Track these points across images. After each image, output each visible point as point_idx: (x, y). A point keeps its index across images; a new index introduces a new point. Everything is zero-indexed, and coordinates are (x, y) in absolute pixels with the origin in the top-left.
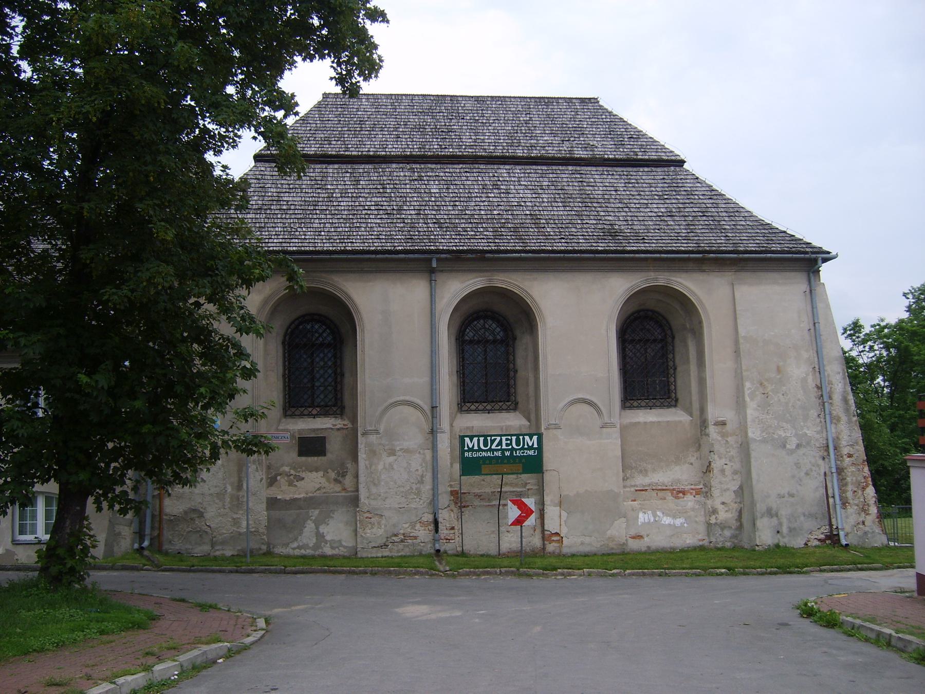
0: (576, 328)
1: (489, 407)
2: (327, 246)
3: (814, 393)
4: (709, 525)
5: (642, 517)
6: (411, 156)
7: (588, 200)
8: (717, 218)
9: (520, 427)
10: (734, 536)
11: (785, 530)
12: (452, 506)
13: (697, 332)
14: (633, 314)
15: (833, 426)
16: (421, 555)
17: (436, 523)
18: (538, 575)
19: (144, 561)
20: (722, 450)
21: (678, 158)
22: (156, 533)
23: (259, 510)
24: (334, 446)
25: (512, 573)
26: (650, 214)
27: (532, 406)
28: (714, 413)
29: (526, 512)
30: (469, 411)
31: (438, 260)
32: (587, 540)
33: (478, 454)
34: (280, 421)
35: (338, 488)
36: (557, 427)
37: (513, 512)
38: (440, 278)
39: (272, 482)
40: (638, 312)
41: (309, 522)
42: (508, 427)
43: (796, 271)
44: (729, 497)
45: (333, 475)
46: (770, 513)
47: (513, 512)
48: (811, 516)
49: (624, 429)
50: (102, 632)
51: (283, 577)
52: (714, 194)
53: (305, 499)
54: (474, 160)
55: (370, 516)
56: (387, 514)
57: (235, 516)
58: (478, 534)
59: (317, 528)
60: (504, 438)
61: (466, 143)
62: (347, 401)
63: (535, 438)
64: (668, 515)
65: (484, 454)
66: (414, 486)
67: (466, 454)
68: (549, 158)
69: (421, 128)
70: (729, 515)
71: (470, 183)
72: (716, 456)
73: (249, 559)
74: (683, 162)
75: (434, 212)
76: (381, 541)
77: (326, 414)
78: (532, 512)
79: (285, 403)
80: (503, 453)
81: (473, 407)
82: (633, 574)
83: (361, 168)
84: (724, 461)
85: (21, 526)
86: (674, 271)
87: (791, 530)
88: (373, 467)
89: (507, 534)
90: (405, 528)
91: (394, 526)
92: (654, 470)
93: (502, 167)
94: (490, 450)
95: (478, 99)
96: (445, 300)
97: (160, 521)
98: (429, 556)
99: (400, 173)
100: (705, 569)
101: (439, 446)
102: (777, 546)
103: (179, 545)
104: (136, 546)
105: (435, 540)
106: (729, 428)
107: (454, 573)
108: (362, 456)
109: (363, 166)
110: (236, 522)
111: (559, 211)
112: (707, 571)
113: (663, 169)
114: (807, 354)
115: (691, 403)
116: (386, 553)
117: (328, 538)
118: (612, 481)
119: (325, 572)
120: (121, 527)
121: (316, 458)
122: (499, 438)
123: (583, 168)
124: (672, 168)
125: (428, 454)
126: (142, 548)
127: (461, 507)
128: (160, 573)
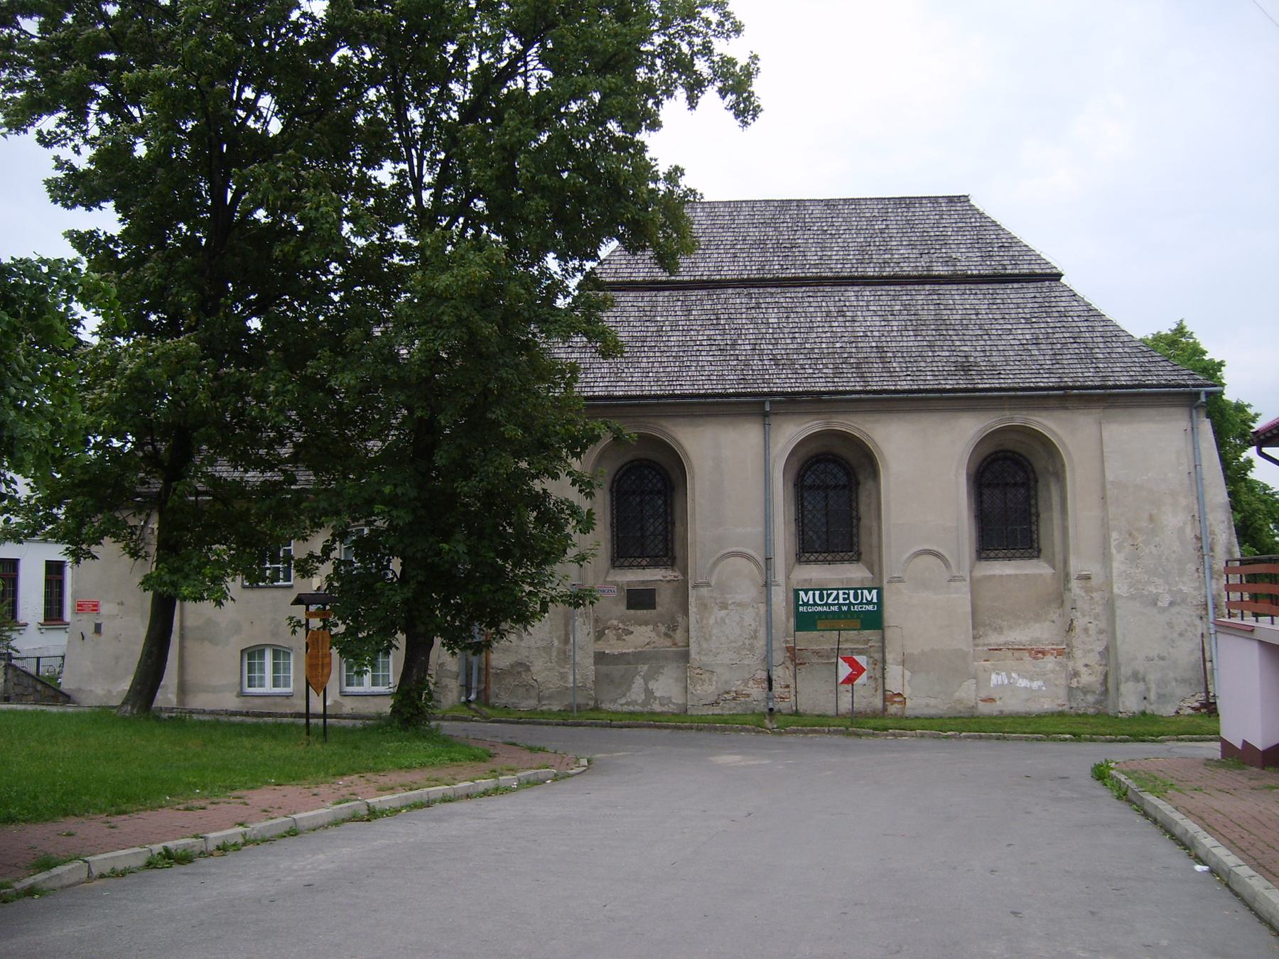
0: (923, 474)
1: (829, 558)
2: (656, 390)
3: (1192, 545)
4: (1070, 689)
5: (995, 679)
6: (749, 280)
7: (943, 327)
8: (1090, 345)
9: (862, 580)
10: (1098, 702)
11: (1153, 696)
12: (788, 663)
13: (1059, 476)
14: (989, 456)
15: (1214, 581)
16: (753, 713)
17: (770, 680)
18: (867, 735)
19: (472, 713)
21: (1055, 271)
22: (483, 686)
23: (588, 667)
24: (665, 599)
25: (841, 732)
27: (875, 557)
28: (1075, 566)
29: (858, 670)
30: (808, 562)
31: (771, 402)
32: (932, 702)
35: (668, 642)
36: (900, 580)
37: (845, 670)
38: (774, 421)
39: (600, 635)
40: (996, 453)
42: (849, 580)
43: (1176, 406)
44: (1093, 659)
45: (663, 629)
46: (1136, 677)
47: (845, 670)
48: (1184, 681)
49: (975, 585)
50: (452, 760)
51: (608, 730)
52: (1092, 314)
53: (634, 654)
54: (819, 281)
56: (718, 670)
58: (814, 693)
59: (646, 684)
61: (810, 261)
62: (678, 553)
63: (874, 592)
64: (1024, 677)
65: (820, 609)
66: (747, 642)
67: (801, 609)
68: (903, 277)
69: (761, 244)
70: (1093, 679)
71: (812, 309)
72: (1078, 614)
73: (576, 714)
74: (1060, 275)
76: (712, 699)
77: (656, 566)
78: (864, 670)
79: (613, 553)
81: (812, 558)
82: (969, 737)
83: (694, 295)
85: (250, 679)
86: (1033, 409)
87: (1160, 696)
90: (737, 685)
91: (726, 682)
92: (1010, 628)
93: (849, 288)
95: (829, 204)
96: (780, 446)
97: (487, 675)
98: (762, 714)
99: (736, 299)
100: (1047, 734)
101: (774, 599)
102: (1144, 713)
103: (504, 699)
104: (463, 699)
105: (769, 699)
106: (1093, 582)
107: (781, 731)
108: (692, 609)
109: (696, 292)
110: (563, 677)
111: (909, 342)
112: (1049, 736)
113: (1035, 285)
115: (1053, 554)
116: (717, 710)
117: (657, 694)
118: (961, 640)
119: (650, 726)
124: (1047, 283)
125: (762, 608)
127: (796, 665)
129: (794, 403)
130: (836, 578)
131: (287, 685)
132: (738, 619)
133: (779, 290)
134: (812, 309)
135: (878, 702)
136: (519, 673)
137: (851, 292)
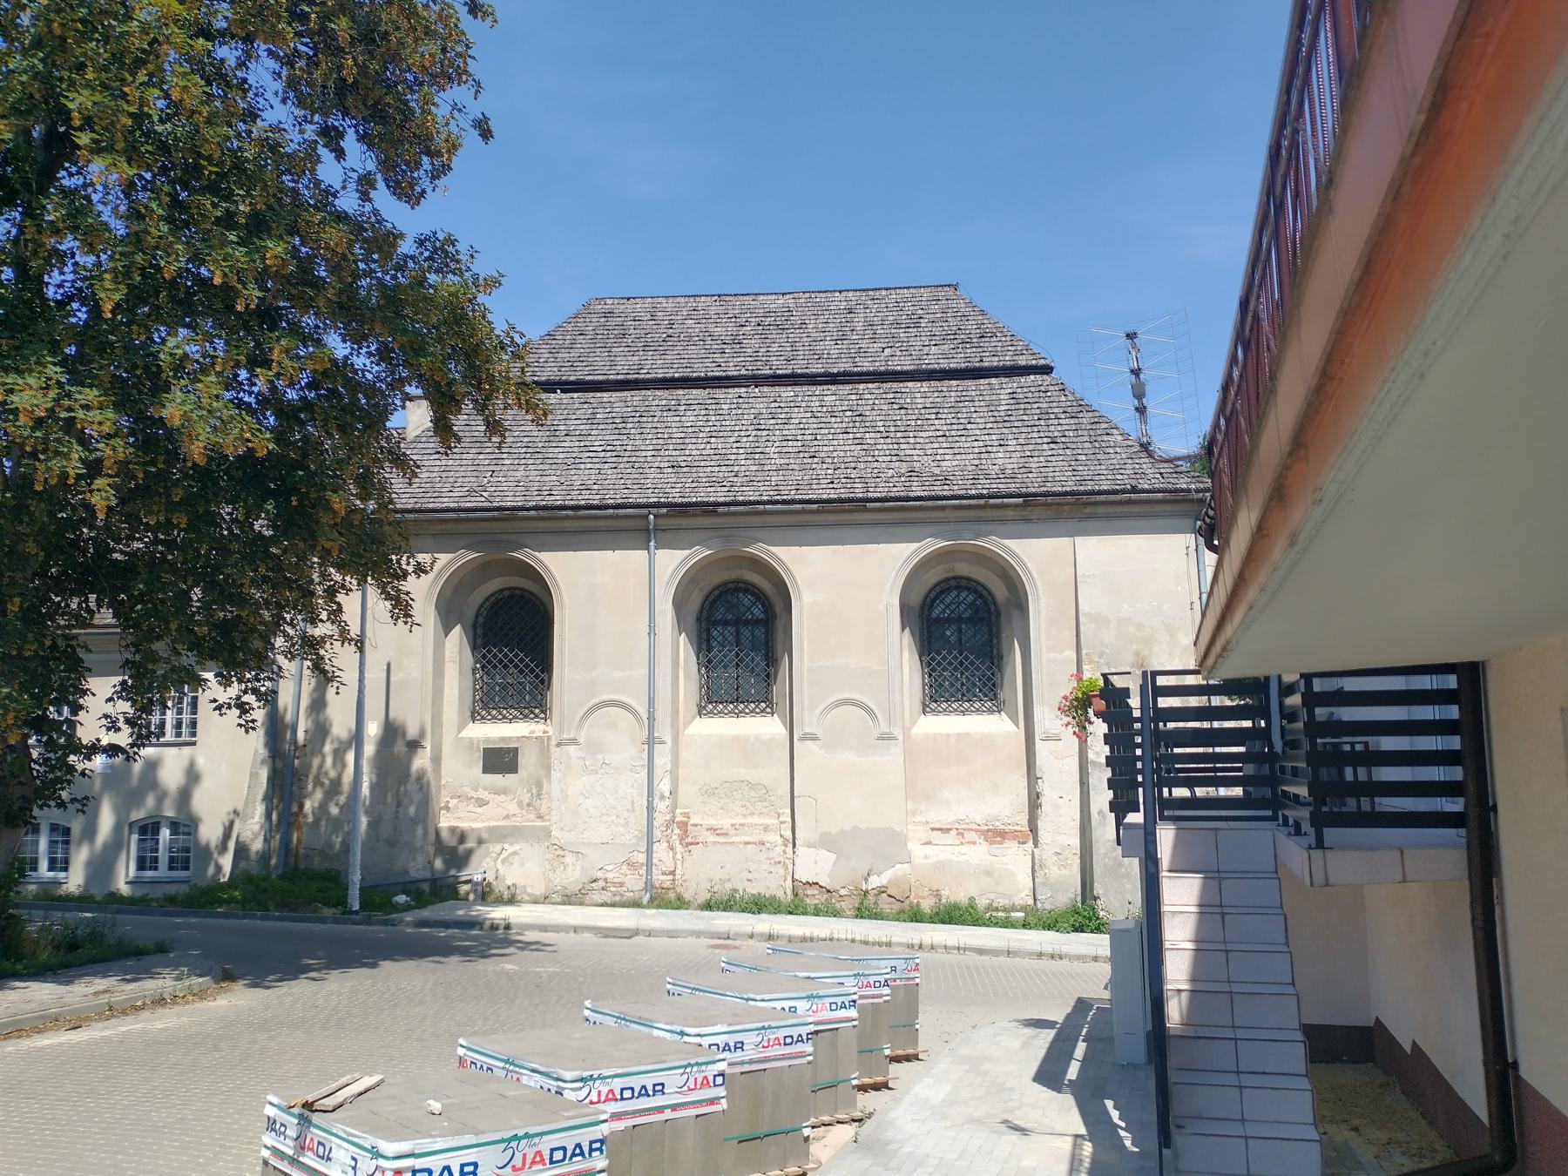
0: (847, 598)
24: (527, 760)
34: (461, 728)
101: (657, 761)
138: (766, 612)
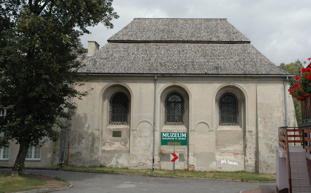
0: (203, 98)
6: (157, 41)
13: (244, 100)
17: (153, 160)
20: (251, 141)
22: (66, 159)
24: (124, 134)
26: (232, 61)
28: (248, 128)
30: (168, 124)
31: (157, 76)
32: (203, 168)
33: (166, 139)
34: (107, 126)
35: (124, 147)
41: (114, 158)
45: (123, 143)
49: (217, 133)
53: (114, 150)
54: (178, 42)
55: (133, 157)
57: (91, 155)
59: (117, 160)
60: (175, 134)
65: (169, 139)
67: (163, 138)
69: (163, 31)
70: (252, 162)
71: (175, 50)
75: (160, 60)
78: (178, 157)
80: (175, 139)
83: (141, 45)
84: (251, 145)
88: (135, 141)
89: (177, 165)
90: (143, 161)
92: (228, 146)
94: (171, 137)
96: (159, 89)
99: (153, 46)
101: (156, 135)
111: (202, 60)
114: (282, 109)
117: (120, 163)
120: (56, 157)
121: (118, 138)
122: (173, 134)
123: (214, 44)
124: (246, 44)
126: (62, 164)
128: (62, 171)
129: (163, 77)
130: (178, 129)
131: (39, 157)
132: (145, 141)
133: (166, 44)
134: (175, 50)
135: (186, 167)
136: (78, 155)
137: (187, 45)
138: (182, 100)
